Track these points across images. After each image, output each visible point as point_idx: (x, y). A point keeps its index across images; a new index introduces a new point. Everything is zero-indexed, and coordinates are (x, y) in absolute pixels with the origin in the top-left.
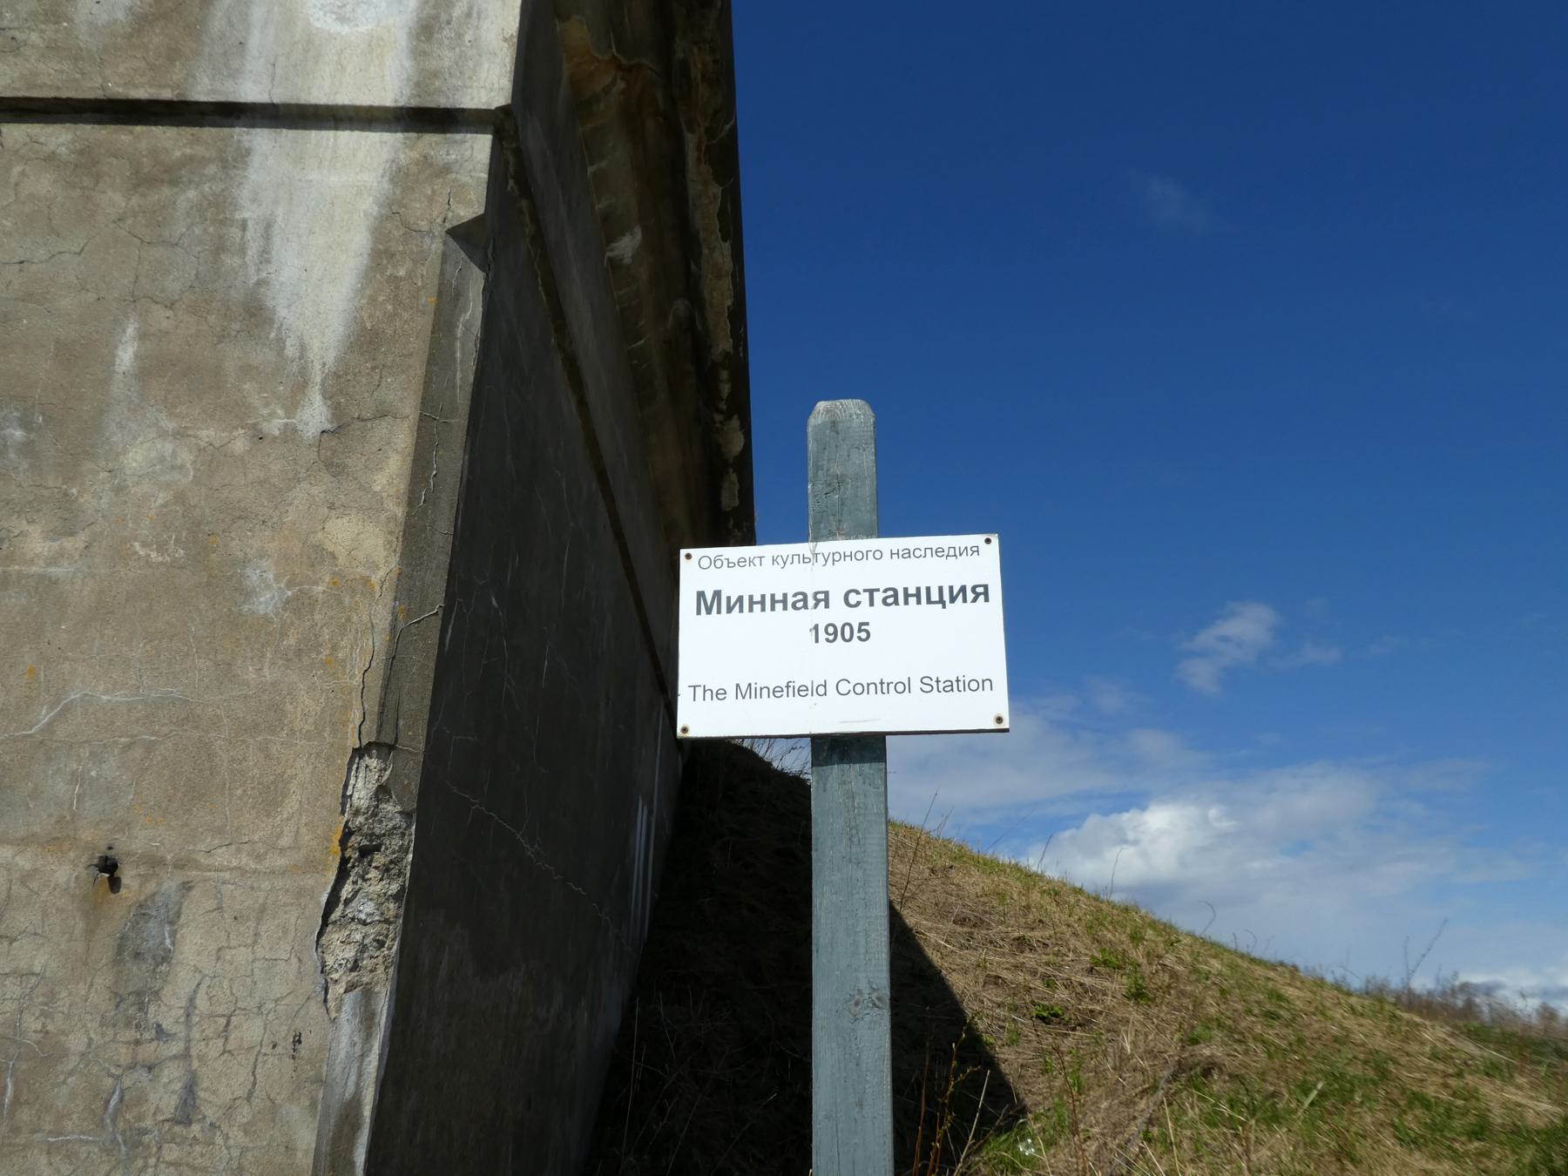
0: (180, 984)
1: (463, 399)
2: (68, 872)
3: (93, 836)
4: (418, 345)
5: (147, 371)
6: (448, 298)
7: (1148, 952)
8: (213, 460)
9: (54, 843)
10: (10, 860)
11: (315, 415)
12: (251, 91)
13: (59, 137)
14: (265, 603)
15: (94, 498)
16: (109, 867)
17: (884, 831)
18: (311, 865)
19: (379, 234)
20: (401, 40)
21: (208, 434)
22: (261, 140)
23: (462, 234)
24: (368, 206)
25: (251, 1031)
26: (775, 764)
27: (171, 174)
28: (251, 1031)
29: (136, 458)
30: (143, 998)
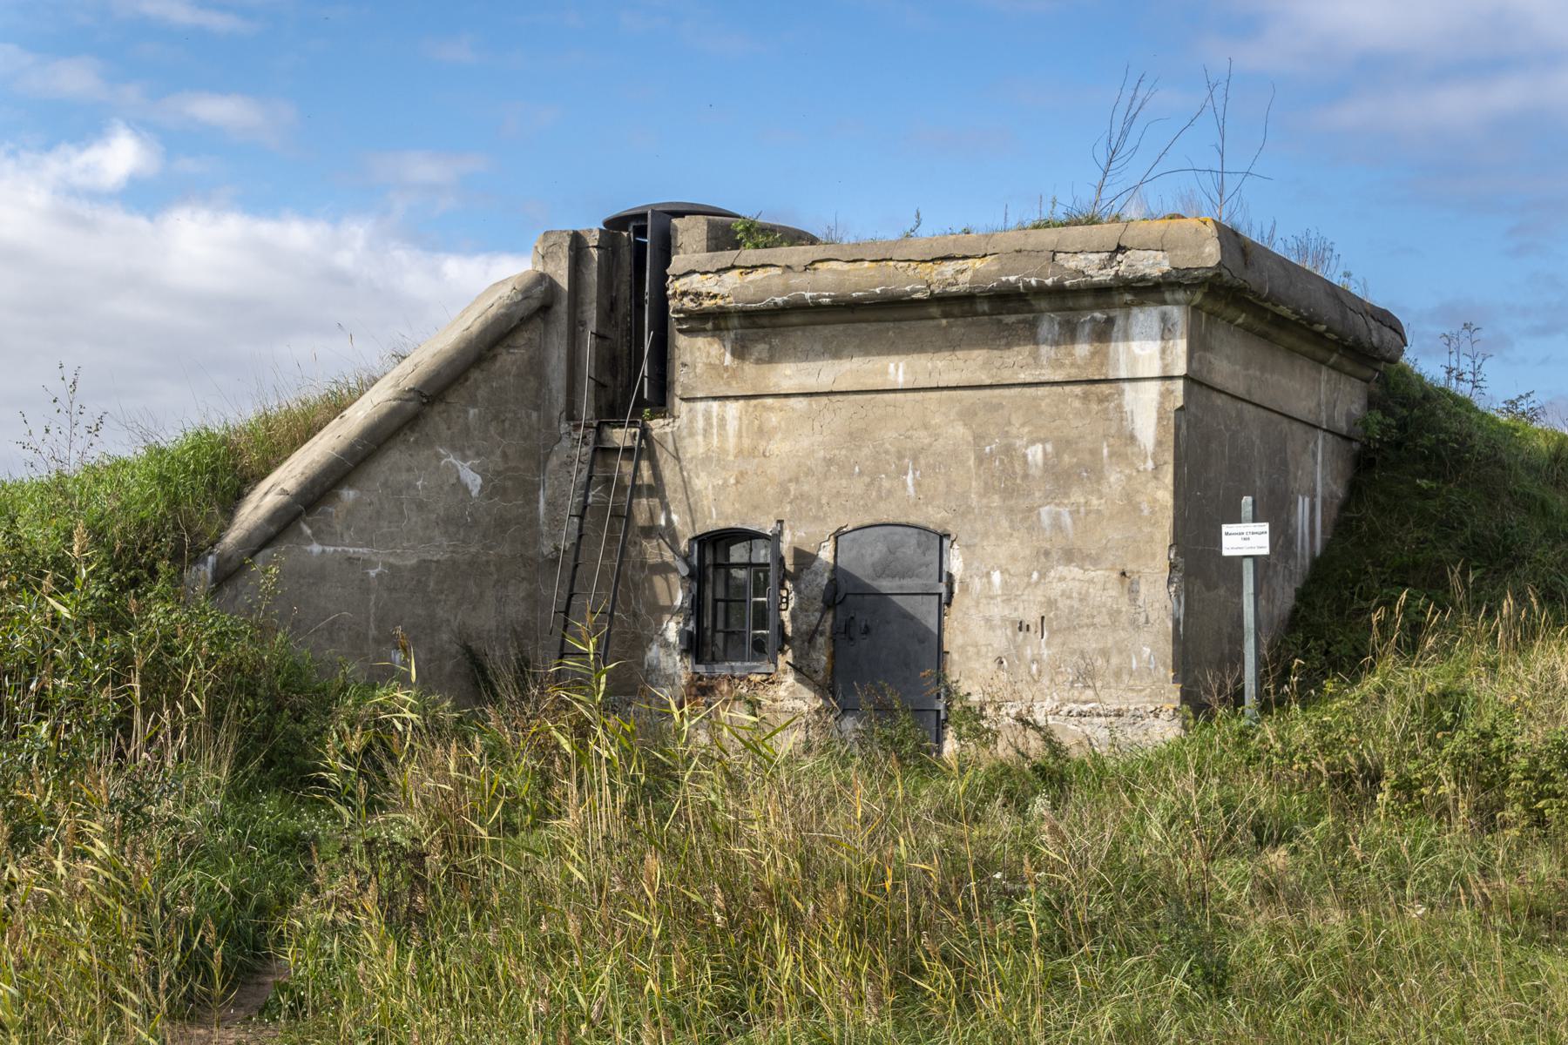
2: (1115, 575)
3: (1119, 567)
5: (1111, 455)
8: (1129, 478)
11: (1150, 465)
13: (1078, 389)
14: (1146, 512)
15: (1105, 490)
19: (1159, 413)
22: (1127, 386)
24: (1155, 404)
25: (1157, 605)
27: (1102, 400)
28: (1157, 605)
29: (1112, 479)
30: (1135, 600)
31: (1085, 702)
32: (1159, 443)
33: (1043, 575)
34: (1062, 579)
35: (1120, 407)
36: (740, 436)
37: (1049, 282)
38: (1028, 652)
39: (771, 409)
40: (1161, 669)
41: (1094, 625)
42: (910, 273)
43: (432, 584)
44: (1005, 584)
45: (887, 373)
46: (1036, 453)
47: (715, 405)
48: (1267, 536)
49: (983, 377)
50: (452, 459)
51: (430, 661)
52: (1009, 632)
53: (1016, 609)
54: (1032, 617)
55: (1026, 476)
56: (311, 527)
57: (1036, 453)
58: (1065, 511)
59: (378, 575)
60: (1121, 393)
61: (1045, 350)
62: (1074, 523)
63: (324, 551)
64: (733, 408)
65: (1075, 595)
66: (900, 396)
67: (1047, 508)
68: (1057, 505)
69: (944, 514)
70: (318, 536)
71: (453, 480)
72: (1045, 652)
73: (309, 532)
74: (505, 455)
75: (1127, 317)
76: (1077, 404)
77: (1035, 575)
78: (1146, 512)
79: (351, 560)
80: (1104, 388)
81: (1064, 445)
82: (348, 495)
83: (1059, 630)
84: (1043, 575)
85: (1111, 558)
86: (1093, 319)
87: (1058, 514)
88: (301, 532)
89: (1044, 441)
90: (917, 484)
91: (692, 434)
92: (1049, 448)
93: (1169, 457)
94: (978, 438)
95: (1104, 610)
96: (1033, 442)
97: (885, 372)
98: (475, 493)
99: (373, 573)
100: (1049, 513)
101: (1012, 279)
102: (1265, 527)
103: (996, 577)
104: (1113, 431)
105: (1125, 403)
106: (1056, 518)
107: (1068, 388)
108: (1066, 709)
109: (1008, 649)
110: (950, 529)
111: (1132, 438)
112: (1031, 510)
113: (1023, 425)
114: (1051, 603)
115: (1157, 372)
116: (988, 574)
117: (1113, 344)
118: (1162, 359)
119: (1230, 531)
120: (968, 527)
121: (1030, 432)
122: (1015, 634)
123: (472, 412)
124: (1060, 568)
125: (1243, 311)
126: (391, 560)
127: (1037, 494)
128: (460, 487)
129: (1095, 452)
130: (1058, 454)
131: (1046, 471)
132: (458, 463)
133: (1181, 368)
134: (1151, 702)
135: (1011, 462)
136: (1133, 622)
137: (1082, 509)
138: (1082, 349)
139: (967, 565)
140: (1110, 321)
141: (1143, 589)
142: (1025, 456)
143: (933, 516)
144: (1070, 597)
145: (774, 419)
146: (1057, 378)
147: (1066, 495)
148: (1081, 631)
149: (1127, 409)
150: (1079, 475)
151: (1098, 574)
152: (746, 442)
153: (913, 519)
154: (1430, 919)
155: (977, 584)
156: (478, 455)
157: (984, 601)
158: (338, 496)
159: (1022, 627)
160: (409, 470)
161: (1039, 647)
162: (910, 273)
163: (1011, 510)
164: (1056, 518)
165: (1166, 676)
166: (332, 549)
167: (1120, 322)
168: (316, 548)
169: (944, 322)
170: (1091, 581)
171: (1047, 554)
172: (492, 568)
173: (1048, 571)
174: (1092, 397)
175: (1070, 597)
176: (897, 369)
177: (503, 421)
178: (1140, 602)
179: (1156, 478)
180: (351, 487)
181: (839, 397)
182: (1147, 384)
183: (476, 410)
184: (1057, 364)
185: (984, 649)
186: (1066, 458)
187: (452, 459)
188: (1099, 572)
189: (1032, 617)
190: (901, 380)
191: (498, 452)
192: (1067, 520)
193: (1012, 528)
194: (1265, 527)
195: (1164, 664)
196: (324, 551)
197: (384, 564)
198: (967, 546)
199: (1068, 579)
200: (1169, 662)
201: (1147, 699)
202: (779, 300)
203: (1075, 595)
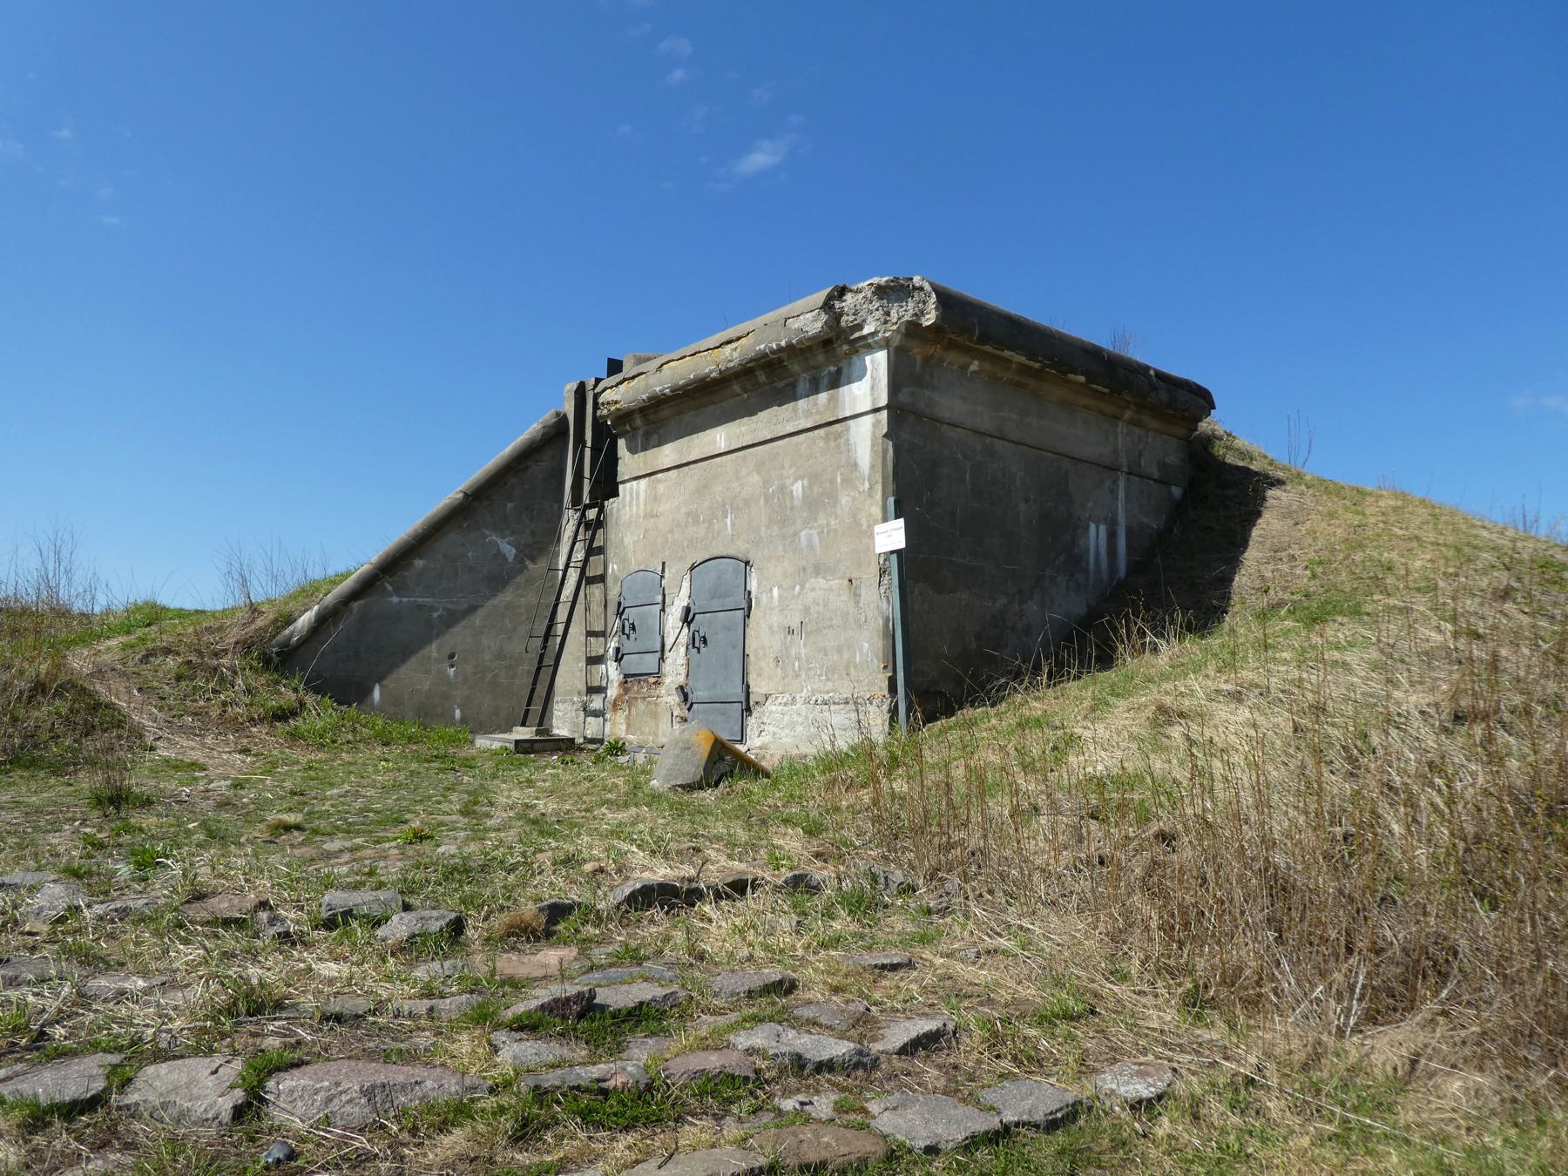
0: (862, 600)
1: (891, 474)
2: (846, 582)
3: (848, 576)
4: (880, 466)
5: (843, 481)
6: (885, 451)
7: (99, 801)
8: (854, 499)
9: (843, 578)
10: (310, 700)
11: (867, 485)
12: (848, 414)
13: (821, 432)
14: (864, 527)
15: (839, 512)
16: (850, 581)
17: (666, 570)
18: (875, 576)
19: (872, 441)
20: (869, 392)
21: (852, 494)
22: (851, 423)
23: (886, 436)
24: (869, 434)
25: (872, 606)
26: (892, 535)
27: (838, 436)
28: (872, 606)
29: (843, 502)
30: (858, 603)
31: (827, 693)
32: (873, 467)
33: (802, 588)
34: (813, 590)
35: (847, 441)
36: (646, 504)
37: (783, 343)
38: (793, 652)
39: (659, 481)
40: (875, 661)
41: (832, 626)
42: (708, 358)
43: (478, 622)
44: (780, 596)
45: (715, 442)
46: (798, 488)
47: (634, 483)
48: (903, 531)
49: (766, 433)
50: (494, 538)
51: (476, 673)
52: (782, 636)
53: (786, 617)
54: (795, 624)
55: (792, 508)
56: (392, 585)
57: (798, 488)
58: (814, 532)
59: (439, 616)
60: (848, 429)
61: (802, 403)
62: (821, 542)
63: (401, 601)
64: (643, 482)
65: (821, 602)
66: (724, 458)
67: (804, 532)
68: (810, 529)
69: (747, 545)
70: (398, 591)
71: (495, 552)
72: (803, 651)
73: (391, 588)
74: (533, 533)
75: (850, 365)
76: (822, 444)
77: (798, 588)
78: (864, 527)
79: (420, 607)
80: (837, 427)
81: (814, 478)
82: (419, 563)
83: (811, 632)
84: (802, 588)
85: (843, 568)
86: (829, 372)
87: (811, 535)
88: (385, 588)
89: (802, 478)
90: (733, 524)
91: (624, 506)
92: (806, 482)
93: (879, 477)
94: (766, 483)
95: (839, 613)
96: (796, 480)
97: (714, 441)
98: (511, 559)
99: (435, 615)
100: (806, 535)
101: (762, 347)
102: (901, 522)
103: (776, 591)
104: (843, 462)
105: (851, 437)
106: (810, 538)
107: (816, 432)
108: (814, 699)
109: (781, 651)
110: (751, 557)
111: (856, 465)
112: (795, 534)
113: (790, 467)
114: (806, 610)
115: (868, 408)
116: (771, 590)
117: (841, 389)
118: (872, 394)
119: (879, 531)
120: (759, 553)
121: (794, 473)
122: (785, 638)
123: (509, 505)
124: (812, 580)
125: (974, 359)
126: (449, 606)
127: (799, 521)
128: (499, 555)
129: (833, 481)
130: (811, 487)
131: (803, 501)
132: (499, 541)
133: (883, 401)
134: (869, 691)
135: (784, 498)
136: (857, 621)
137: (825, 530)
138: (823, 397)
139: (759, 584)
140: (839, 372)
141: (863, 592)
142: (792, 491)
143: (739, 548)
144: (818, 604)
145: (661, 488)
146: (809, 426)
147: (815, 520)
148: (824, 631)
149: (852, 442)
150: (823, 502)
151: (835, 583)
152: (649, 508)
153: (731, 552)
154: (1399, 767)
155: (764, 599)
156: (513, 533)
157: (768, 612)
158: (412, 564)
159: (791, 631)
160: (463, 545)
161: (800, 647)
162: (708, 358)
163: (783, 537)
164: (810, 538)
165: (878, 667)
166: (406, 600)
167: (845, 371)
168: (395, 599)
169: (745, 395)
170: (831, 589)
171: (804, 569)
172: (523, 610)
173: (805, 583)
174: (832, 436)
175: (818, 604)
176: (720, 437)
177: (533, 511)
178: (861, 605)
179: (871, 496)
180: (421, 558)
181: (692, 466)
182: (864, 418)
183: (512, 504)
184: (808, 414)
185: (768, 651)
186: (816, 489)
187: (494, 538)
188: (836, 581)
189: (795, 624)
190: (723, 446)
191: (528, 532)
192: (816, 540)
193: (784, 551)
194: (901, 522)
195: (878, 658)
196: (401, 601)
197: (444, 609)
198: (759, 569)
199: (818, 585)
200: (881, 655)
201: (866, 688)
202: (644, 397)
203: (821, 602)
